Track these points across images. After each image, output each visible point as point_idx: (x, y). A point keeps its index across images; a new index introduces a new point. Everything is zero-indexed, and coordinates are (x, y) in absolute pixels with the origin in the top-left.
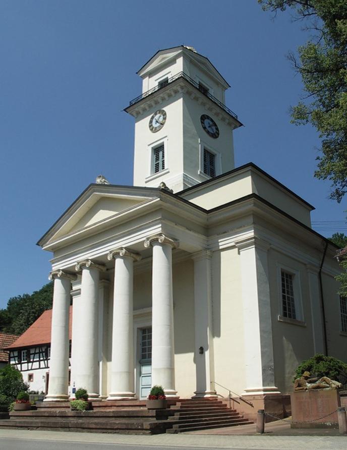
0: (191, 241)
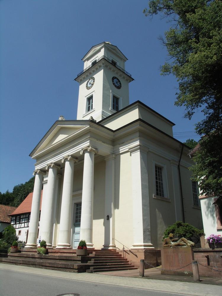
0: (105, 149)
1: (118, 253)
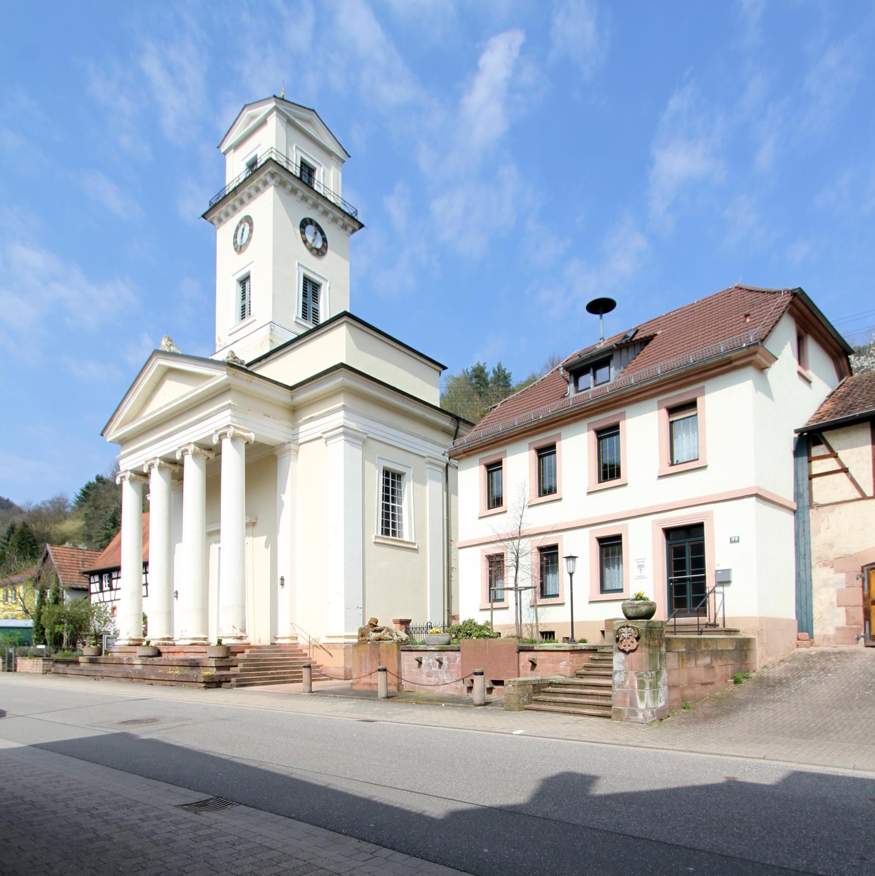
0: (271, 430)
1: (301, 650)
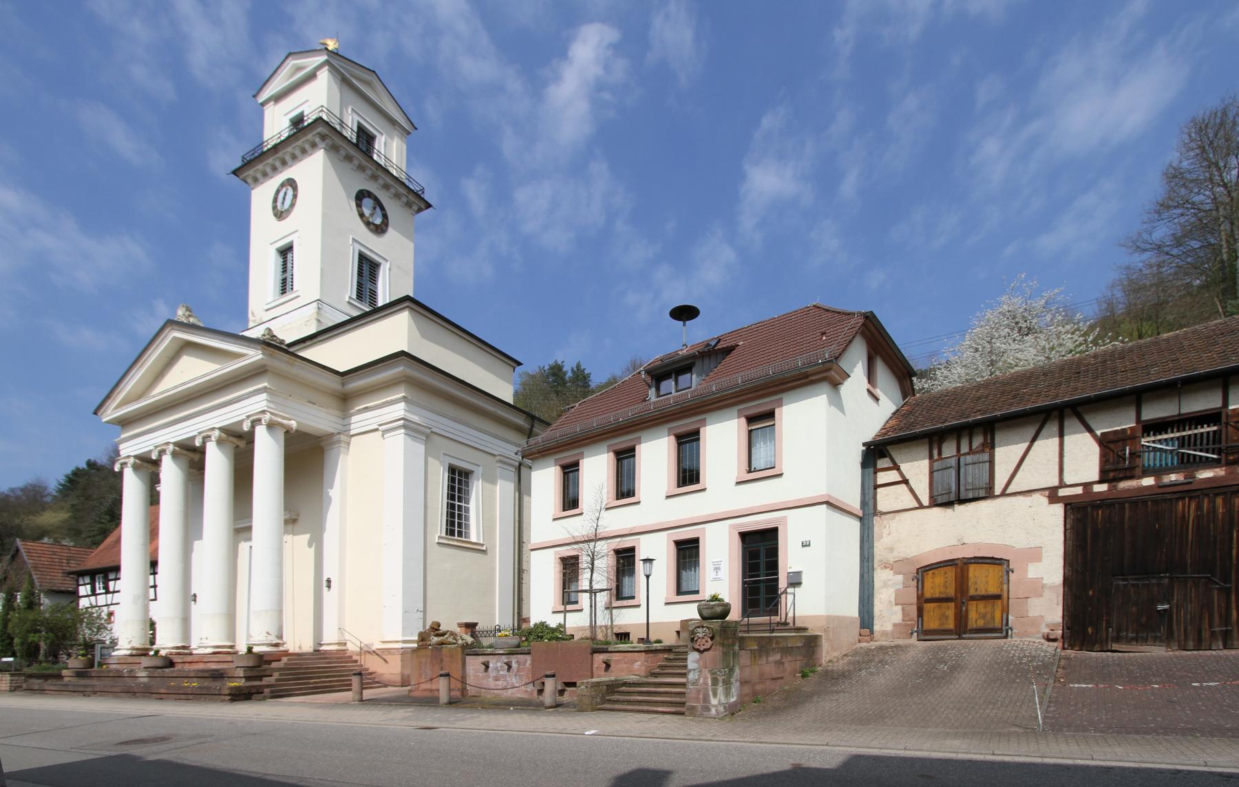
0: (318, 419)
